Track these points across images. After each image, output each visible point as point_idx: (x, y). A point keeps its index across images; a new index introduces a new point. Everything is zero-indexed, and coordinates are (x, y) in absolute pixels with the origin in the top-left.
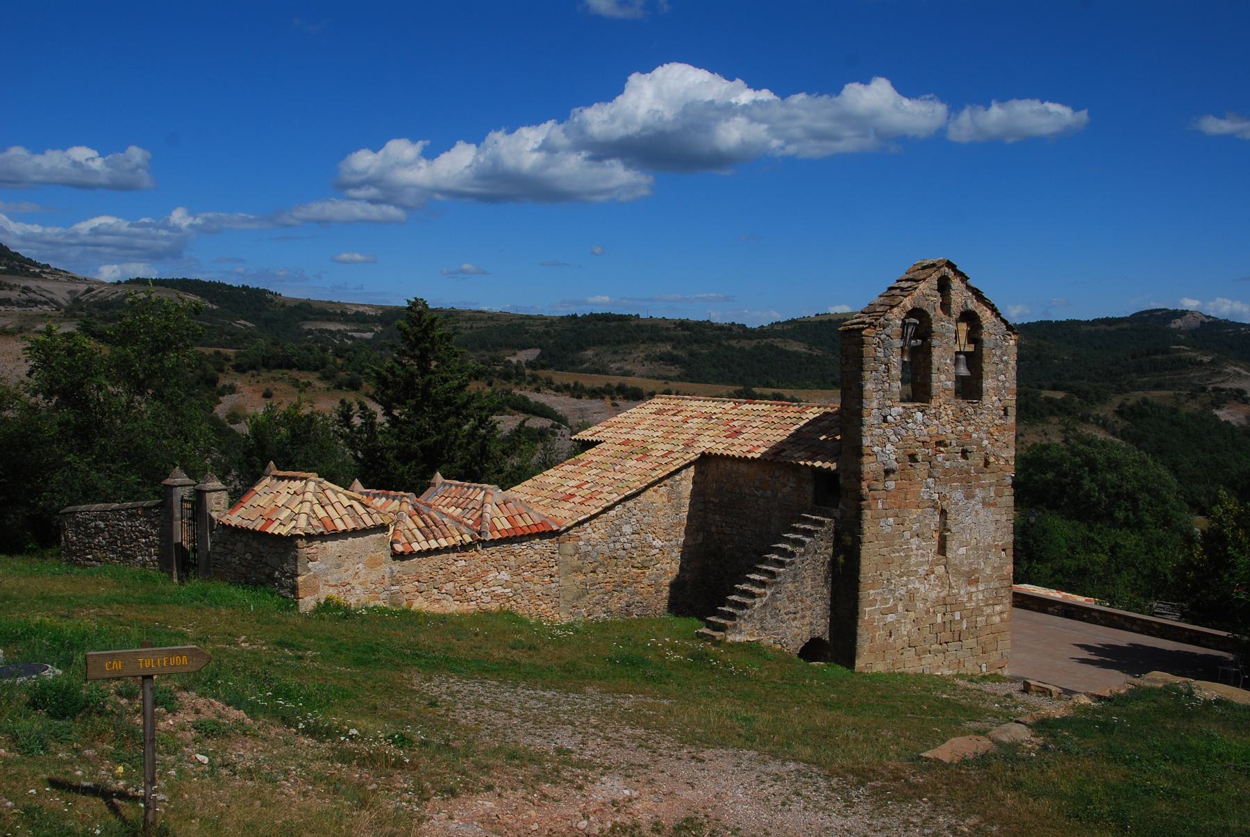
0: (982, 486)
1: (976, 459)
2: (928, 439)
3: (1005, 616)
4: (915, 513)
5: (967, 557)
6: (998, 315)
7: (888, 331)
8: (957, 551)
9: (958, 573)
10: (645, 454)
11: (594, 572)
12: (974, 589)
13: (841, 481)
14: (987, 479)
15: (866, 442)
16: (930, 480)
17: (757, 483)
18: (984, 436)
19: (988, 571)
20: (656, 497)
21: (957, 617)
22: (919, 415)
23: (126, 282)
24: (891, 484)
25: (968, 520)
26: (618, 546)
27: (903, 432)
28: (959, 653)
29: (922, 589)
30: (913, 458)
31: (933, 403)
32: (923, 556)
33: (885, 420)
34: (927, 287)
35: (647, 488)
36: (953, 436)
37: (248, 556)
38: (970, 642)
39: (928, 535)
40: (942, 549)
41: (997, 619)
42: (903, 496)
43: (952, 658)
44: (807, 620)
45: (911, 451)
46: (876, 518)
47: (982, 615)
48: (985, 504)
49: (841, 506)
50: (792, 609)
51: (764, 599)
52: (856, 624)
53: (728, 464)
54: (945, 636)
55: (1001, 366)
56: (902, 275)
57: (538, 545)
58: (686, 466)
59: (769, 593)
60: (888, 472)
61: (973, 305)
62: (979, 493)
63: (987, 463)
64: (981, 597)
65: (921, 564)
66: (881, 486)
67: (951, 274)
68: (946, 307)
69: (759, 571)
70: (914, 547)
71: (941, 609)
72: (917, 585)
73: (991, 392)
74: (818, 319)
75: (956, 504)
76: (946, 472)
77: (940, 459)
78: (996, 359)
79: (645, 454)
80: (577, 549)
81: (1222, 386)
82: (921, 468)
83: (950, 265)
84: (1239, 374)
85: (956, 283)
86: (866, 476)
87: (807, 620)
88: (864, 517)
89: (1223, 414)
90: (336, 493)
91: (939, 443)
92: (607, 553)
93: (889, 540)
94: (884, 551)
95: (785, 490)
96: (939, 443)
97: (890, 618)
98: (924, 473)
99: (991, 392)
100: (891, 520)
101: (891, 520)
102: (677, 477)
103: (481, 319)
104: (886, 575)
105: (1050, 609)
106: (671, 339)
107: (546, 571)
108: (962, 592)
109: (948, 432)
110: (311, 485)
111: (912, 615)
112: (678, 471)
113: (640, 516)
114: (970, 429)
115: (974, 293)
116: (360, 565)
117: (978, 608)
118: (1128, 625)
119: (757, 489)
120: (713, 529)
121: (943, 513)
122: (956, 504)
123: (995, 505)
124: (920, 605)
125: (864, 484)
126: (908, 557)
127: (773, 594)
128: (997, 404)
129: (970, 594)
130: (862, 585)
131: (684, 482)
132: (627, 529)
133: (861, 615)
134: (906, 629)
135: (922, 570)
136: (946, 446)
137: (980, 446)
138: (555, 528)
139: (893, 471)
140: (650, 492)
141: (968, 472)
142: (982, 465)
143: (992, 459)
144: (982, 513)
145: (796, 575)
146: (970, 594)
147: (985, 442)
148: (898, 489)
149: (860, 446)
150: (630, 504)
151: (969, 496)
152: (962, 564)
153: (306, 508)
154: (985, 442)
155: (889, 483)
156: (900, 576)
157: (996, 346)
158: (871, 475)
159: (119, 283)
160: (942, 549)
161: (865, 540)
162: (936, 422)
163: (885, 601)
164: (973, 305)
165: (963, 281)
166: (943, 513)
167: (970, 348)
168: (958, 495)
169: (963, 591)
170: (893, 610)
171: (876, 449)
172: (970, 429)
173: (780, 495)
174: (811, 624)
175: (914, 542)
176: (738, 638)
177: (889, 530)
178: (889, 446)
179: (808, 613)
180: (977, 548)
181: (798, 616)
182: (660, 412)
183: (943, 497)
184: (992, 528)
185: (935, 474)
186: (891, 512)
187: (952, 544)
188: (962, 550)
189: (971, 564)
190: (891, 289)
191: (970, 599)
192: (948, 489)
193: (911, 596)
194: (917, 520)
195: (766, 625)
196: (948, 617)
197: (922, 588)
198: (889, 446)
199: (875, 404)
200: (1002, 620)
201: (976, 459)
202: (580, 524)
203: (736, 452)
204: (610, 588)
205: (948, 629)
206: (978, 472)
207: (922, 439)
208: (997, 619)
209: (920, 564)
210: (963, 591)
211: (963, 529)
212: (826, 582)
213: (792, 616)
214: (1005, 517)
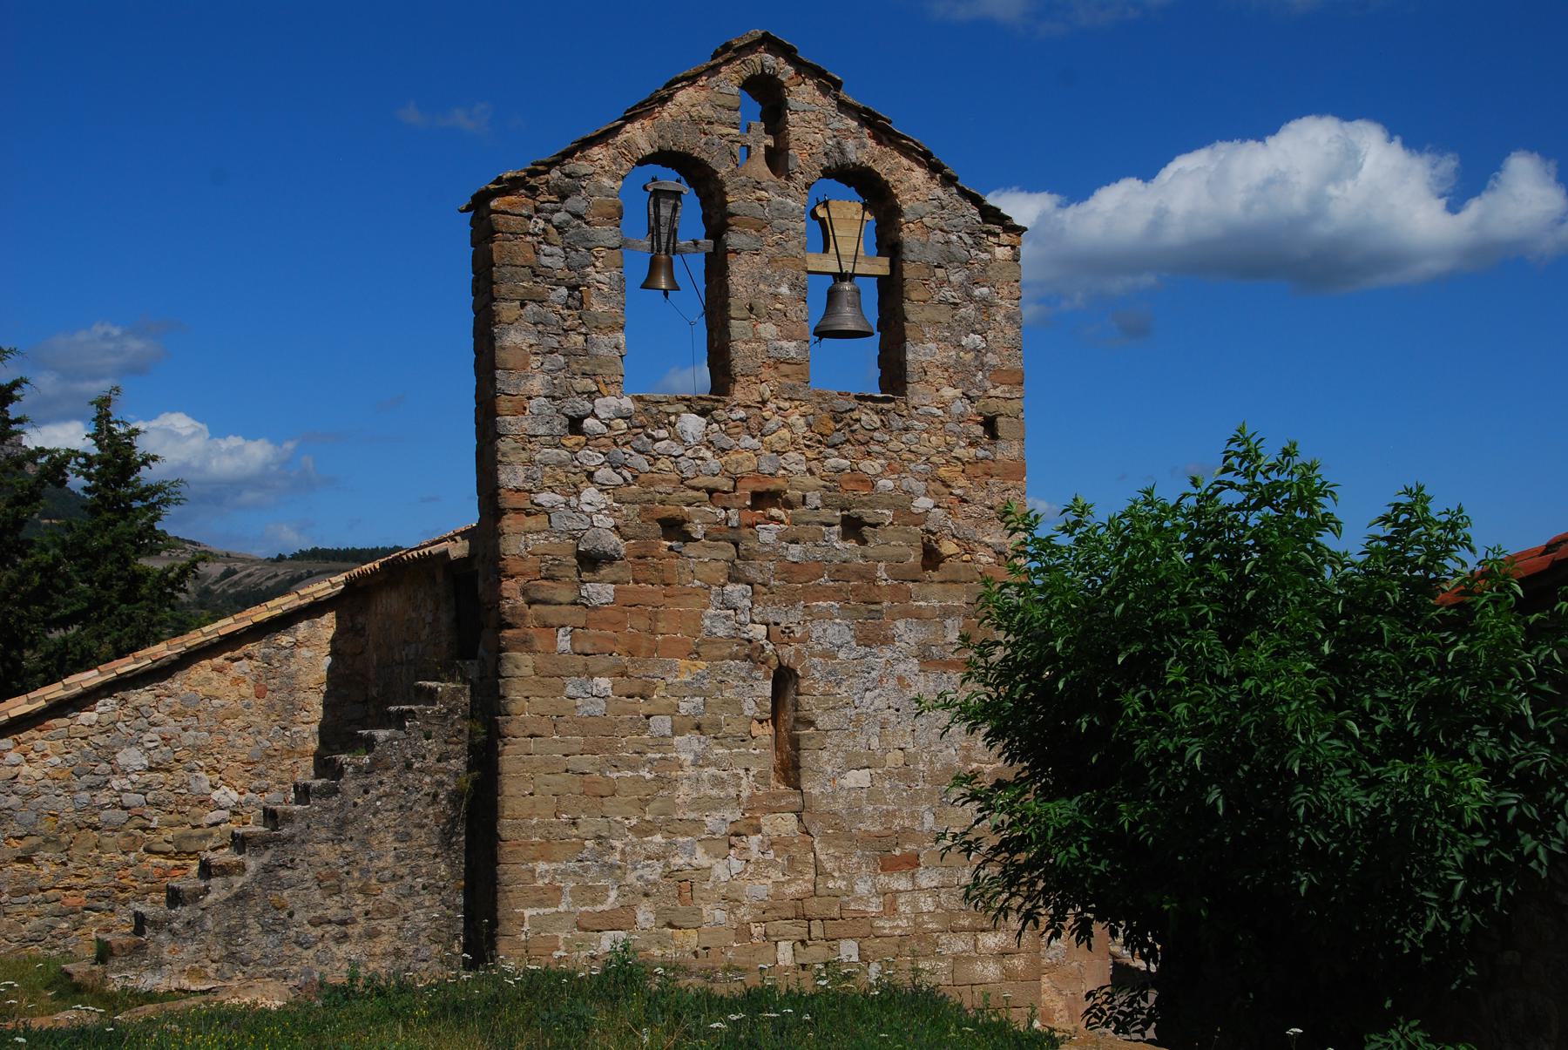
0: (918, 615)
1: (894, 545)
4: (685, 671)
5: (873, 795)
6: (949, 181)
7: (574, 203)
8: (837, 779)
9: (841, 833)
11: (26, 859)
12: (901, 883)
14: (931, 597)
16: (735, 591)
18: (920, 486)
20: (220, 684)
23: (295, 557)
24: (600, 591)
25: (873, 701)
26: (103, 797)
27: (641, 462)
29: (720, 870)
30: (674, 528)
33: (575, 425)
36: (809, 480)
39: (737, 728)
40: (790, 770)
42: (642, 623)
44: (384, 943)
45: (670, 511)
46: (552, 675)
51: (238, 882)
55: (968, 311)
58: (313, 610)
59: (253, 864)
60: (590, 561)
61: (862, 150)
63: (932, 557)
65: (716, 804)
66: (563, 593)
67: (786, 71)
70: (688, 758)
73: (936, 375)
75: (828, 655)
76: (790, 571)
78: (947, 293)
85: (803, 96)
86: (512, 565)
87: (384, 943)
88: (508, 669)
91: (762, 499)
92: (69, 815)
93: (600, 736)
94: (583, 762)
96: (762, 499)
98: (719, 570)
99: (936, 375)
101: (603, 683)
102: (285, 639)
104: (590, 824)
108: (862, 888)
112: (285, 622)
113: (171, 727)
114: (871, 466)
115: (864, 123)
121: (784, 679)
124: (714, 914)
125: (510, 588)
127: (267, 869)
128: (958, 407)
129: (890, 900)
130: (505, 849)
131: (304, 652)
132: (131, 757)
133: (505, 927)
136: (788, 505)
137: (904, 513)
139: (610, 559)
140: (202, 670)
141: (869, 577)
142: (915, 558)
143: (948, 547)
145: (342, 824)
147: (922, 503)
148: (626, 604)
151: (873, 637)
152: (856, 812)
155: (590, 589)
156: (643, 830)
157: (949, 260)
159: (281, 558)
160: (790, 770)
161: (513, 727)
162: (748, 441)
163: (597, 895)
164: (862, 150)
165: (824, 90)
167: (882, 266)
168: (835, 631)
172: (871, 466)
174: (398, 953)
175: (687, 747)
176: (149, 981)
177: (599, 708)
179: (388, 925)
181: (354, 930)
185: (752, 573)
188: (857, 778)
189: (890, 815)
192: (797, 614)
193: (684, 884)
194: (694, 689)
198: (590, 494)
199: (537, 384)
200: (1009, 975)
204: (72, 900)
206: (902, 576)
211: (857, 722)
212: (446, 840)
213: (334, 930)
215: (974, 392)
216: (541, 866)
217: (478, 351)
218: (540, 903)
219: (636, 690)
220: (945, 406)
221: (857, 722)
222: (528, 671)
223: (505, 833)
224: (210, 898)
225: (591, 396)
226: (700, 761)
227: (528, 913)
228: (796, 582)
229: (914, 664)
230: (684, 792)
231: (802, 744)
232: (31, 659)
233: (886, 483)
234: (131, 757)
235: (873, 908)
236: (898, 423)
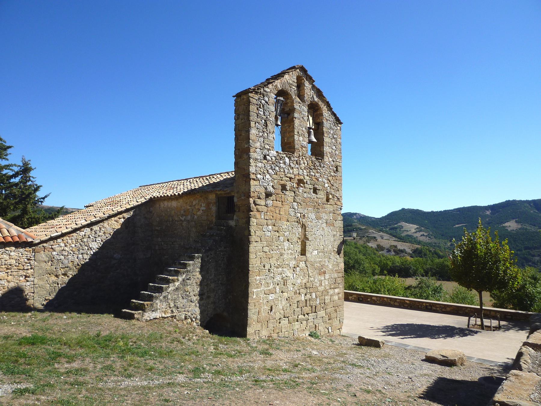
2: (293, 176)
3: (340, 295)
8: (312, 253)
13: (235, 200)
15: (252, 169)
16: (295, 204)
17: (182, 212)
19: (330, 267)
21: (314, 296)
22: (287, 160)
25: (318, 233)
27: (277, 168)
28: (315, 320)
30: (284, 188)
31: (296, 155)
32: (292, 254)
33: (265, 158)
34: (290, 79)
35: (110, 217)
38: (322, 313)
40: (303, 252)
41: (336, 298)
43: (312, 324)
49: (235, 217)
51: (177, 284)
52: (247, 303)
54: (307, 309)
57: (13, 252)
59: (180, 279)
64: (327, 283)
68: (301, 96)
82: (289, 195)
83: (303, 69)
85: (307, 84)
88: (251, 223)
89: (370, 245)
95: (199, 213)
97: (271, 297)
98: (291, 199)
105: (350, 297)
107: (21, 272)
109: (304, 175)
119: (182, 216)
121: (304, 227)
127: (183, 280)
133: (250, 295)
134: (282, 305)
135: (293, 263)
138: (30, 240)
143: (331, 197)
144: (326, 229)
149: (248, 174)
150: (96, 228)
158: (256, 194)
160: (303, 252)
162: (297, 166)
166: (304, 227)
168: (313, 216)
169: (317, 279)
173: (196, 217)
175: (286, 244)
178: (268, 176)
185: (298, 200)
188: (316, 252)
191: (321, 285)
192: (306, 211)
195: (179, 304)
196: (308, 296)
201: (322, 195)
202: (52, 239)
205: (308, 305)
207: (289, 175)
208: (336, 298)
210: (317, 279)
215: (334, 160)
217: (238, 130)
218: (257, 288)
219: (277, 230)
220: (330, 162)
222: (255, 224)
223: (250, 269)
224: (170, 289)
225: (269, 150)
227: (255, 290)
228: (305, 202)
229: (325, 225)
232: (355, 296)
235: (318, 285)
236: (322, 166)
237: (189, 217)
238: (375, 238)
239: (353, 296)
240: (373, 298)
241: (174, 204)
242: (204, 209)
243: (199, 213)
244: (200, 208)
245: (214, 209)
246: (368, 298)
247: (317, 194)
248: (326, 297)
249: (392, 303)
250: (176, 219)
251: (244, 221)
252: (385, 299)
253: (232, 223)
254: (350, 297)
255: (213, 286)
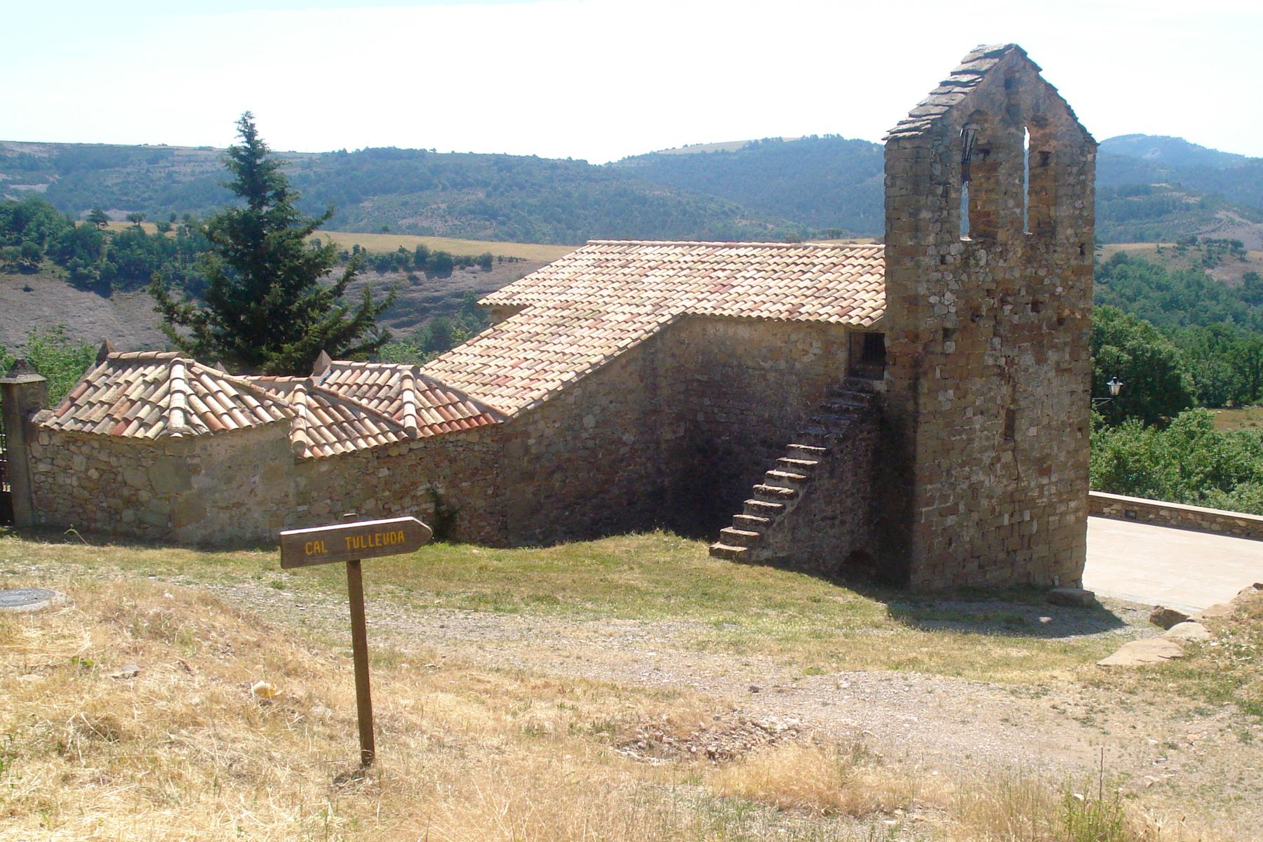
0: (1054, 346)
8: (1028, 432)
10: (597, 317)
13: (887, 343)
14: (1061, 338)
16: (997, 341)
19: (1062, 457)
21: (1027, 518)
24: (951, 347)
25: (1040, 391)
29: (987, 483)
32: (988, 438)
33: (943, 261)
37: (94, 474)
40: (1010, 430)
47: (1054, 514)
48: (1060, 370)
49: (886, 375)
50: (829, 514)
53: (721, 327)
56: (957, 66)
60: (947, 334)
62: (1052, 356)
69: (784, 466)
70: (978, 427)
71: (1010, 508)
72: (982, 477)
74: (686, 151)
76: (1015, 328)
77: (1007, 312)
79: (597, 317)
80: (527, 450)
81: (1214, 236)
82: (986, 325)
84: (1232, 222)
89: (1216, 274)
90: (215, 378)
94: (944, 435)
95: (805, 359)
97: (951, 520)
100: (951, 392)
103: (206, 160)
105: (1106, 510)
106: (485, 184)
108: (1033, 484)
110: (179, 371)
111: (975, 516)
114: (1042, 272)
116: (257, 479)
117: (1051, 505)
118: (1205, 524)
119: (765, 359)
120: (701, 417)
122: (1026, 370)
123: (1069, 370)
124: (984, 503)
126: (970, 441)
132: (531, 441)
135: (987, 458)
144: (1055, 382)
146: (1041, 487)
153: (179, 400)
154: (1059, 290)
156: (962, 465)
160: (1010, 430)
163: (945, 498)
168: (1028, 359)
169: (1032, 482)
170: (953, 511)
171: (933, 300)
175: (978, 422)
177: (948, 406)
178: (948, 295)
179: (849, 518)
180: (1048, 426)
181: (837, 522)
182: (598, 264)
183: (1011, 362)
184: (1067, 400)
186: (949, 382)
187: (1022, 423)
188: (1033, 431)
189: (1043, 448)
190: (944, 84)
192: (1016, 351)
193: (974, 490)
196: (1017, 518)
197: (988, 481)
198: (948, 295)
201: (1049, 313)
203: (731, 310)
206: (1051, 327)
209: (983, 450)
210: (1032, 482)
214: (1081, 388)
216: (929, 487)
218: (927, 505)
220: (1068, 239)
221: (1034, 404)
226: (983, 429)
230: (976, 444)
231: (921, 419)
233: (1047, 281)
234: (531, 441)
237: (782, 365)
238: (1237, 245)
239: (1115, 507)
240: (1162, 513)
241: (744, 332)
242: (817, 351)
243: (805, 359)
244: (810, 354)
245: (842, 355)
246: (1148, 513)
247: (1038, 312)
248: (1051, 519)
249: (1205, 524)
250: (750, 363)
251: (906, 383)
252: (1190, 516)
253: (880, 386)
254: (1106, 510)
255: (849, 502)
